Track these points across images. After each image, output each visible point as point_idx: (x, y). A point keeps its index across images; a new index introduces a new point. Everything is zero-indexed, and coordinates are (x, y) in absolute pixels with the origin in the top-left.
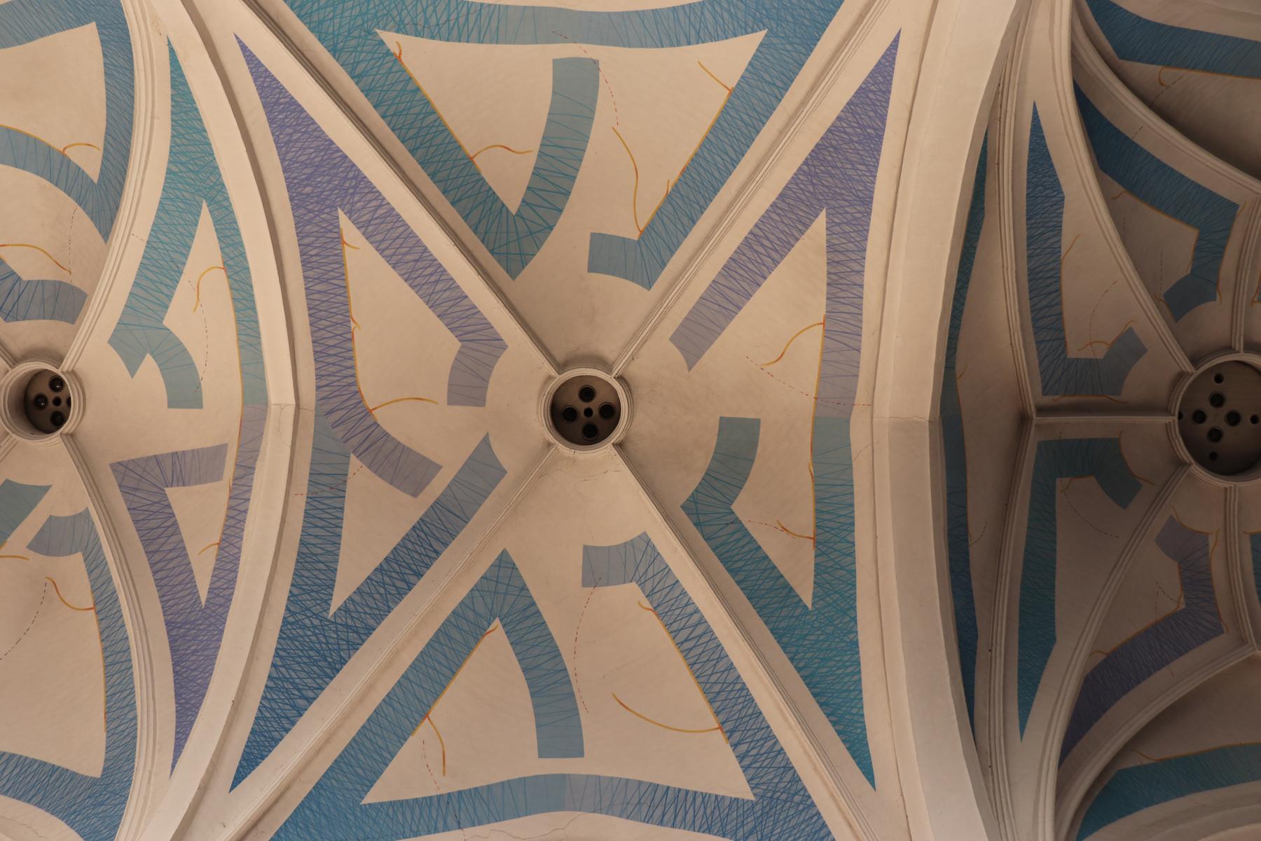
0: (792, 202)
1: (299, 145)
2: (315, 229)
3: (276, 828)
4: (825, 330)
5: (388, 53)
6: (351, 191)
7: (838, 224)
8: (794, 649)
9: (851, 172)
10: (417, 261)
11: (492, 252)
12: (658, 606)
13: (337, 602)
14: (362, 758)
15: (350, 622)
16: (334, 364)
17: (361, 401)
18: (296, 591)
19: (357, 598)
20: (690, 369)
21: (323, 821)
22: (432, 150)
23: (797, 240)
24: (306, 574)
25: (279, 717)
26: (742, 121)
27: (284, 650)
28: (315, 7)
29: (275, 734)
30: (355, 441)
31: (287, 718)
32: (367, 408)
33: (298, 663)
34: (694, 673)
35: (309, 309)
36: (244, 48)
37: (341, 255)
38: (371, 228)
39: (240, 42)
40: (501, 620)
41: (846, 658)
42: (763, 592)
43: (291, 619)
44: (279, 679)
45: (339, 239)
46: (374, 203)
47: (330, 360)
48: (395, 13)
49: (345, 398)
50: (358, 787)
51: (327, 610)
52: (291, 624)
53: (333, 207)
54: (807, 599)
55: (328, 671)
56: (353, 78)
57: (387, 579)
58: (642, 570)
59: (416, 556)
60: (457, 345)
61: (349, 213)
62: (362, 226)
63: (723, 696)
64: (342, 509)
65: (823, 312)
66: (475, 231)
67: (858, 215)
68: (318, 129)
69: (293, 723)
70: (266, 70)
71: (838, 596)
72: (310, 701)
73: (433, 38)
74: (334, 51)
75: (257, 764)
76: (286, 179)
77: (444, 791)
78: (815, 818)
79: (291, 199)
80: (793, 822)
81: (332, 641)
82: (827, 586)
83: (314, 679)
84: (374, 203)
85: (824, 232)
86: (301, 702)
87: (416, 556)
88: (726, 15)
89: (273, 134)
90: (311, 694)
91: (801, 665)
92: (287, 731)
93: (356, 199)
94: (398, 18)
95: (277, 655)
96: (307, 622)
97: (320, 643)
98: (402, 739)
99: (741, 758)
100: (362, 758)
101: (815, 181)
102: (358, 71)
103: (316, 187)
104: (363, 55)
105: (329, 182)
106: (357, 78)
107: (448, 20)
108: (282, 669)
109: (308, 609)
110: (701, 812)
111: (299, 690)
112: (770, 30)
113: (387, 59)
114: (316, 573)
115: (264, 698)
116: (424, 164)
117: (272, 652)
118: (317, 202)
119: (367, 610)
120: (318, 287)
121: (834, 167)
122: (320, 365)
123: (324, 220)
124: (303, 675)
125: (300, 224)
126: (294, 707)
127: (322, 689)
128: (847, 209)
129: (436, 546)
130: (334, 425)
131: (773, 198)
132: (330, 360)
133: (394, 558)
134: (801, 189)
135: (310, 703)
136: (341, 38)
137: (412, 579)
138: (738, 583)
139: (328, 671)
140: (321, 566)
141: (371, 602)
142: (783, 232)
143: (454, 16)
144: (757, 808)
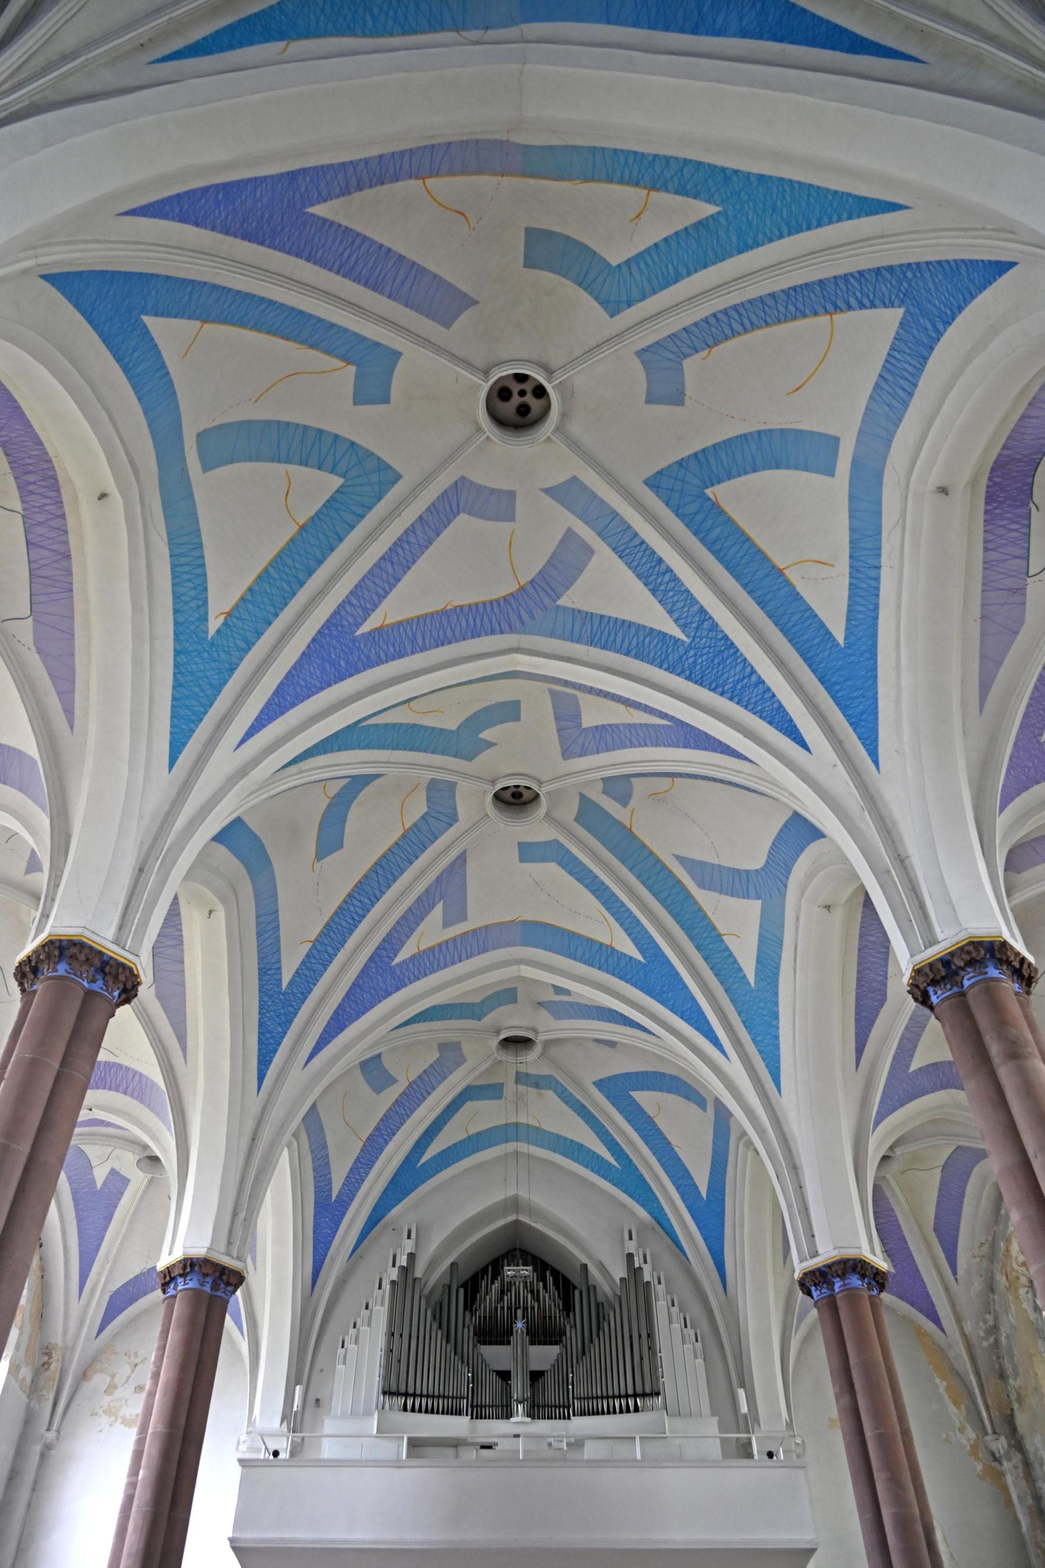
0: (303, 242)
1: (308, 679)
2: (373, 651)
3: (847, 724)
4: (431, 176)
5: (225, 624)
6: (340, 628)
7: (319, 194)
8: (760, 235)
9: (265, 200)
10: (392, 563)
11: (380, 499)
12: (706, 344)
13: (677, 633)
14: (806, 637)
15: (694, 625)
16: (482, 621)
17: (512, 595)
18: (665, 666)
19: (676, 615)
20: (476, 302)
21: (849, 683)
22: (298, 566)
23: (340, 225)
24: (652, 654)
25: (762, 698)
26: (230, 305)
27: (711, 683)
28: (201, 694)
29: (775, 705)
30: (546, 601)
31: (764, 693)
32: (518, 590)
33: (723, 674)
34: (774, 324)
35: (438, 646)
36: (243, 741)
37: (392, 626)
38: (368, 606)
39: (239, 746)
40: (707, 487)
41: (775, 190)
42: (700, 251)
43: (687, 673)
44: (733, 692)
45: (379, 630)
46: (348, 608)
47: (479, 625)
48: (193, 627)
49: (510, 610)
50: (830, 645)
51: (683, 642)
52: (691, 673)
53: (354, 640)
54: (711, 209)
55: (732, 651)
56: (250, 649)
57: (662, 587)
58: (671, 356)
59: (644, 560)
60: (463, 517)
61: (358, 625)
62: (367, 613)
63: (800, 306)
64: (602, 616)
65: (412, 182)
66: (362, 517)
67: (308, 179)
68: (294, 667)
69: (769, 689)
70: (256, 720)
71: (710, 181)
72: (753, 671)
73: (206, 589)
74: (232, 669)
75: (795, 726)
76: (336, 683)
77: (847, 570)
78: (931, 267)
79: (351, 675)
80: (931, 285)
81: (708, 643)
82: (699, 187)
83: (737, 664)
84: (348, 608)
85: (329, 203)
86: (754, 678)
87: (644, 560)
88: (136, 355)
89: (302, 701)
90: (748, 670)
91: (777, 233)
92: (774, 696)
93: (345, 623)
94: (197, 623)
95: (714, 690)
96: (691, 660)
97: (708, 653)
98: (797, 597)
99: (862, 306)
100: (806, 637)
101: (279, 229)
102: (243, 645)
103: (340, 657)
104: (231, 645)
105: (335, 648)
106: (250, 645)
107: (189, 580)
108: (726, 688)
109: (681, 657)
110: (907, 357)
111: (744, 678)
112: (141, 313)
113: (230, 623)
114: (652, 645)
115: (746, 707)
116: (310, 573)
117: (712, 694)
118: (352, 654)
119: (686, 609)
120: (420, 641)
121: (262, 216)
122: (483, 632)
123: (365, 645)
124: (732, 673)
125: (370, 665)
126: (756, 685)
127: (745, 660)
128: (303, 190)
129: (636, 542)
130: (533, 618)
131: (301, 262)
132: (479, 625)
133: (597, 1133)
134: (289, 239)
135: (755, 672)
136: (221, 667)
137: (663, 567)
138: (689, 274)
139: (732, 651)
140: (648, 639)
141: (680, 605)
142: (334, 240)
143: (185, 577)
144: (912, 309)
